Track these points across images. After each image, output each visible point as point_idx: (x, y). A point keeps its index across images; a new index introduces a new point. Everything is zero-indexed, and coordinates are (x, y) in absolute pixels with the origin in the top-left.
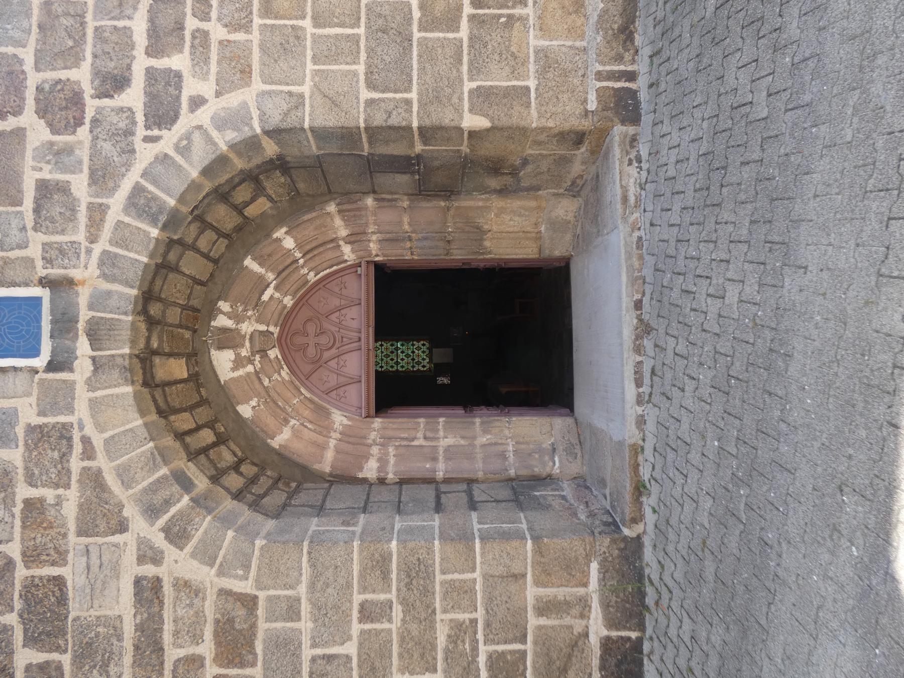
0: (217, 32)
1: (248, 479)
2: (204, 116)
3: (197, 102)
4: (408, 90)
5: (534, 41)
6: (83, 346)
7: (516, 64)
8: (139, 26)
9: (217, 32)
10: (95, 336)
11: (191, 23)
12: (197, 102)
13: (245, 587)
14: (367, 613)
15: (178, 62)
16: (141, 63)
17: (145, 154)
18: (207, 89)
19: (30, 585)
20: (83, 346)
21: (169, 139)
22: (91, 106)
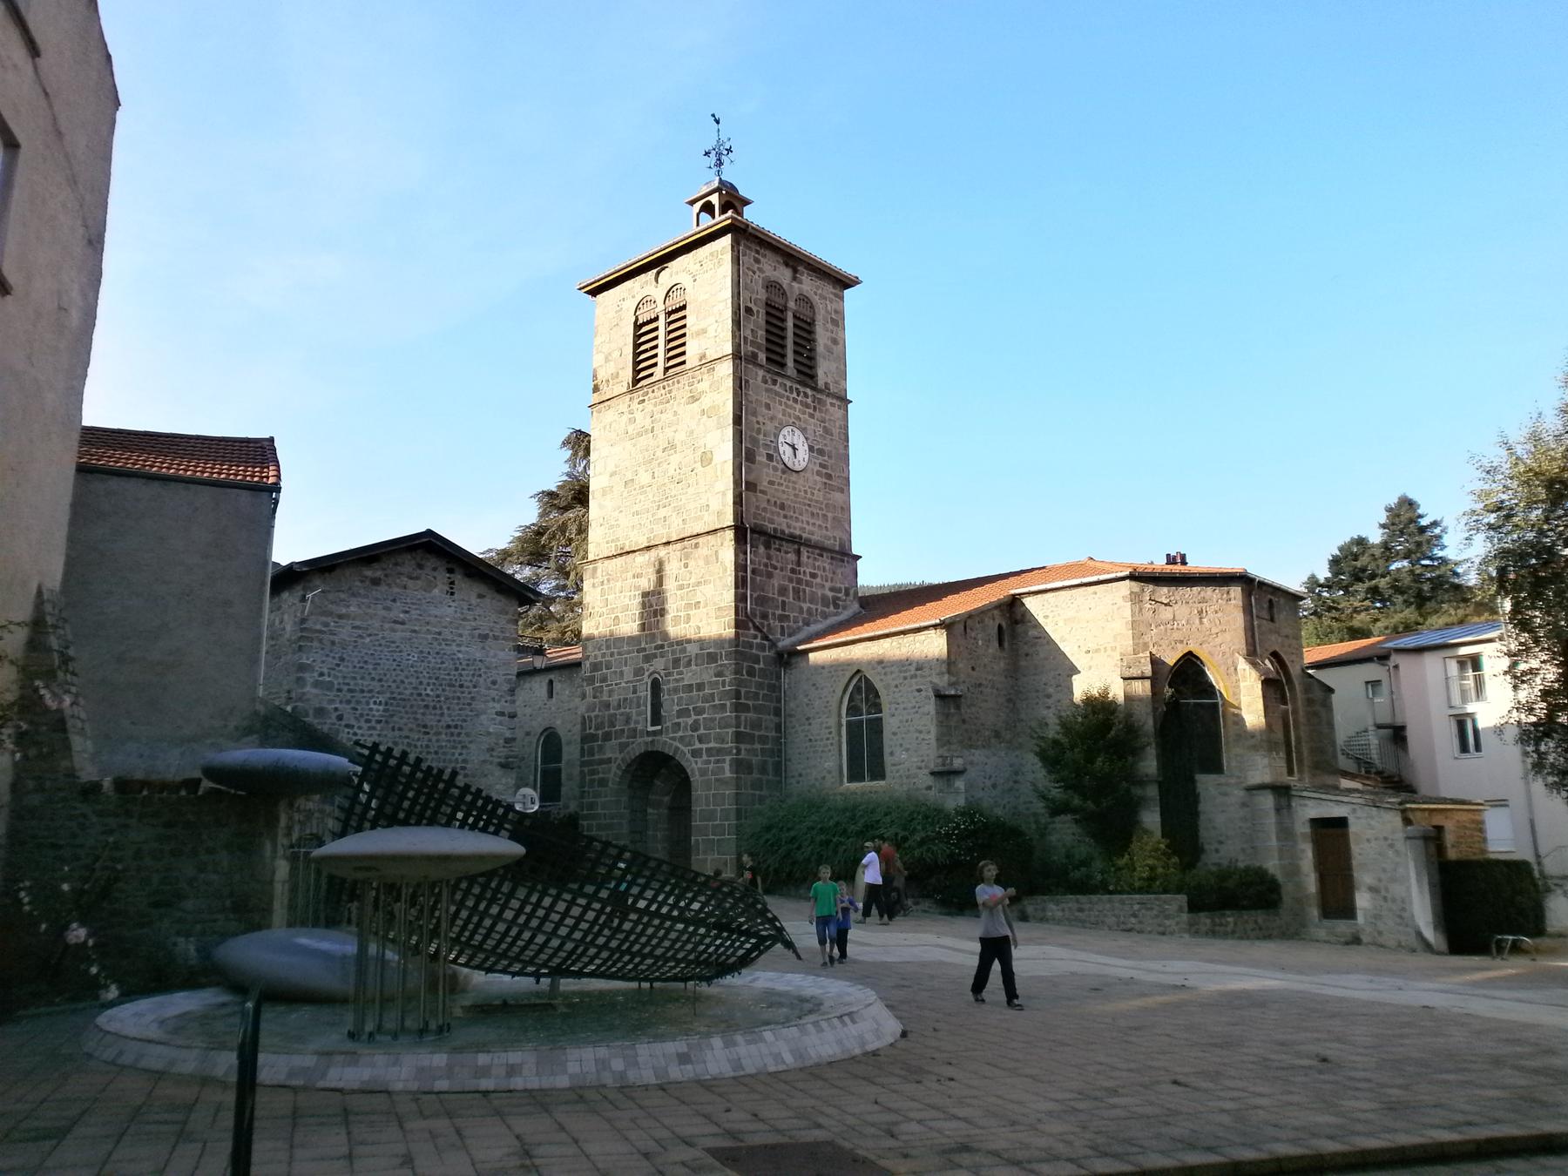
0: (711, 766)
1: (507, 908)
2: (694, 765)
3: (696, 763)
4: (705, 729)
5: (709, 858)
6: (650, 739)
7: (705, 852)
8: (712, 745)
9: (711, 766)
10: (652, 742)
11: (712, 759)
12: (696, 763)
13: (610, 784)
14: (724, 682)
15: (705, 757)
16: (704, 746)
17: (686, 750)
18: (700, 765)
19: (756, 688)
20: (650, 739)
21: (689, 756)
22: (695, 734)
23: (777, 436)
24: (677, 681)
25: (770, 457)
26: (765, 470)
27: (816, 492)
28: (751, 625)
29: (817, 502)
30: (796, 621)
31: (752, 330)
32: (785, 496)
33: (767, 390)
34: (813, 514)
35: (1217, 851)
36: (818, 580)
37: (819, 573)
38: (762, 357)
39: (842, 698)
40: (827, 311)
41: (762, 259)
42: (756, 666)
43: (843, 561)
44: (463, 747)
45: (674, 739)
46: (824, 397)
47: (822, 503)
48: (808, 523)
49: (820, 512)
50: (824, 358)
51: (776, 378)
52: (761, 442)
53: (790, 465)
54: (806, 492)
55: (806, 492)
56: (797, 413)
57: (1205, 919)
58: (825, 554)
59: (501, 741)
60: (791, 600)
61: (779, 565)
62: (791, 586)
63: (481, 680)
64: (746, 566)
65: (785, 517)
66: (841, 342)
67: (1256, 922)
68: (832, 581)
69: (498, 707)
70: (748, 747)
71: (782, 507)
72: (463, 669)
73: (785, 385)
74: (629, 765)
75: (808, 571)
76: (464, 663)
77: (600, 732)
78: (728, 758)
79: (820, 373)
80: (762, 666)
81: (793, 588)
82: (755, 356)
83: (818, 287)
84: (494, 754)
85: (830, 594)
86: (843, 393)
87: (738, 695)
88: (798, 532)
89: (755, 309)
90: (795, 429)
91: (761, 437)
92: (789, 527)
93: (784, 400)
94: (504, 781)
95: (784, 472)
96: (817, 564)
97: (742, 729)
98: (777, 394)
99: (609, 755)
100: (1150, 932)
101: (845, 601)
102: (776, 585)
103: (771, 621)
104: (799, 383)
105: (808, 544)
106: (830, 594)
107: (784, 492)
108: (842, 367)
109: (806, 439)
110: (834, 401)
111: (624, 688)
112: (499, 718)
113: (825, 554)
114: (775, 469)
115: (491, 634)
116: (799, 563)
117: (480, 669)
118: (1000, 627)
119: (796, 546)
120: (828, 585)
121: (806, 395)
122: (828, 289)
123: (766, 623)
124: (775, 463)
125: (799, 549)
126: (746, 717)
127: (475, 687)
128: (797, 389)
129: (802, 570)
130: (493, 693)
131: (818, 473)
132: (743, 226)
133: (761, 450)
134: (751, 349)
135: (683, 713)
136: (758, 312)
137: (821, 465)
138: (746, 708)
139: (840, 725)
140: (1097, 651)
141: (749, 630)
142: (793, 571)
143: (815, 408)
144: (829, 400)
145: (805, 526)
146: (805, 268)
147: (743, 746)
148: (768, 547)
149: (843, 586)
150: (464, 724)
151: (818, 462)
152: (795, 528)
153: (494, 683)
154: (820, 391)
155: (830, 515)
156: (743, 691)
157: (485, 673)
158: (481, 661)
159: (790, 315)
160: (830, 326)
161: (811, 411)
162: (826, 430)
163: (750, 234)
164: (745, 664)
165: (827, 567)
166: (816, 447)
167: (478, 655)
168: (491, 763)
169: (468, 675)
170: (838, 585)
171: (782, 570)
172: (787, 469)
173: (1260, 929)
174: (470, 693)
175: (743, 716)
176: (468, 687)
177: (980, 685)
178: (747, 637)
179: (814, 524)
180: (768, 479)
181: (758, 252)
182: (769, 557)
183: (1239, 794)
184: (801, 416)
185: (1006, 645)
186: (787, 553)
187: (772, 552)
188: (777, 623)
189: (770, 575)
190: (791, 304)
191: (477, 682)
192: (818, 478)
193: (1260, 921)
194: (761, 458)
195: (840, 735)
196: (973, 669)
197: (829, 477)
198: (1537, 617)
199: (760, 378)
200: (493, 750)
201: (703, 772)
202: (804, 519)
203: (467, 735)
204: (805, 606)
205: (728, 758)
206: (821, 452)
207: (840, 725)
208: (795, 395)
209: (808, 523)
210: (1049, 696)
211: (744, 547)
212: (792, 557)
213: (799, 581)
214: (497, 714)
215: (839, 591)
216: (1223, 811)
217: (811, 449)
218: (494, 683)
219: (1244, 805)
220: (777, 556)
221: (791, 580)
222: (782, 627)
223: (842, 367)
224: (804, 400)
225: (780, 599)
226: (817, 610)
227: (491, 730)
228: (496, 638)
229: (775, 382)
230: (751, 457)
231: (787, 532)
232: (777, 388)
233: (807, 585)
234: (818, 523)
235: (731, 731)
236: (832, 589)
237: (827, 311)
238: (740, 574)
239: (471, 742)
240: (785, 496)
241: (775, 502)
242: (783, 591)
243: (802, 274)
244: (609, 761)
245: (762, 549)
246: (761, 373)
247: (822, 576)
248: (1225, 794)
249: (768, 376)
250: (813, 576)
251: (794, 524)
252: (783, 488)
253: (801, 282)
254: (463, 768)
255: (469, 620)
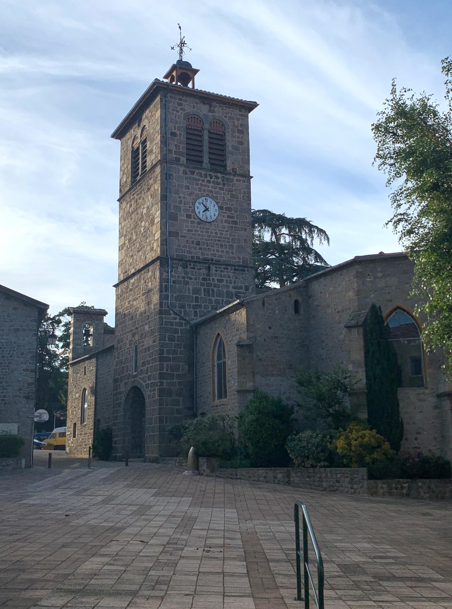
6: (133, 379)
23: (194, 204)
24: (142, 346)
25: (189, 216)
26: (185, 224)
27: (224, 233)
28: (171, 312)
29: (225, 238)
30: (206, 307)
31: (176, 145)
32: (200, 237)
33: (186, 178)
34: (221, 245)
35: (416, 439)
36: (224, 283)
37: (225, 279)
38: (183, 160)
39: (214, 350)
40: (234, 125)
41: (184, 103)
42: (176, 335)
43: (227, 269)
44: (3, 389)
45: (140, 379)
46: (232, 177)
47: (229, 239)
48: (218, 251)
49: (227, 244)
50: (232, 154)
51: (193, 170)
52: (182, 208)
53: (204, 219)
54: (216, 233)
55: (216, 233)
56: (210, 189)
57: (382, 485)
58: (229, 268)
59: (26, 385)
60: (203, 296)
61: (193, 277)
62: (202, 288)
63: (15, 353)
64: (168, 279)
65: (200, 249)
66: (246, 143)
67: (429, 487)
68: (235, 283)
69: (25, 366)
70: (169, 381)
71: (198, 243)
72: (4, 348)
73: (201, 174)
74: (128, 395)
75: (216, 278)
76: (5, 344)
77: (119, 377)
78: (157, 388)
79: (229, 163)
80: (180, 335)
81: (204, 289)
82: (177, 160)
83: (227, 113)
84: (22, 391)
85: (233, 291)
86: (247, 173)
87: (161, 352)
88: (210, 257)
89: (178, 133)
90: (208, 198)
91: (182, 205)
92: (202, 254)
93: (201, 182)
94: (27, 406)
95: (199, 223)
96: (223, 274)
97: (165, 371)
98: (194, 179)
99: (122, 390)
100: (347, 492)
101: (245, 293)
102: (191, 288)
103: (187, 309)
104: (211, 171)
105: (218, 263)
106: (233, 291)
107: (199, 235)
108: (247, 158)
109: (217, 203)
110: (240, 178)
111: (127, 352)
112: (24, 372)
113: (229, 268)
114: (192, 222)
115: (21, 328)
116: (209, 275)
117: (14, 347)
118: (296, 302)
119: (207, 265)
120: (231, 285)
121: (217, 178)
122: (236, 112)
123: (183, 310)
124: (192, 219)
125: (209, 267)
126: (167, 365)
127: (11, 357)
128: (209, 175)
129: (211, 278)
130: (22, 360)
131: (226, 221)
132: (165, 86)
133: (182, 212)
134: (175, 156)
135: (144, 364)
136: (180, 134)
137: (228, 217)
138: (168, 359)
139: (213, 366)
140: (343, 311)
141: (170, 314)
142: (204, 279)
143: (224, 184)
144: (235, 178)
145: (215, 252)
146: (217, 103)
147: (165, 381)
148: (185, 267)
149: (243, 285)
150: (4, 377)
151: (226, 215)
152: (208, 255)
153: (22, 354)
154: (229, 174)
155: (235, 245)
156: (165, 349)
157: (17, 349)
158: (15, 343)
159: (206, 133)
160: (237, 134)
161: (221, 186)
162: (233, 196)
163: (171, 89)
164: (167, 334)
165: (231, 275)
166: (225, 207)
167: (13, 340)
168: (20, 397)
169: (7, 351)
170: (240, 285)
171: (196, 279)
172: (201, 222)
173: (433, 492)
174: (8, 360)
175: (165, 364)
176: (7, 357)
177: (276, 337)
178: (168, 318)
179: (222, 251)
180: (187, 229)
181: (180, 99)
182: (186, 273)
183: (433, 400)
184: (213, 190)
185: (302, 312)
186: (200, 269)
187: (188, 270)
188: (191, 309)
189: (186, 283)
190: (207, 126)
191: (13, 354)
192: (226, 224)
193: (433, 486)
194: (182, 217)
195: (213, 373)
196: (270, 328)
197: (235, 223)
198: (409, 250)
199: (181, 172)
200: (21, 390)
201: (149, 396)
202: (215, 249)
203: (6, 382)
204: (213, 299)
205: (157, 388)
206: (229, 209)
207: (213, 366)
208: (209, 178)
209: (218, 251)
210: (323, 342)
211: (166, 269)
212: (204, 271)
213: (209, 285)
214: (24, 370)
215: (241, 288)
216: (421, 412)
217: (221, 208)
218: (22, 354)
219: (436, 407)
220: (192, 272)
221: (202, 285)
222: (196, 312)
223: (247, 158)
224: (216, 180)
225: (194, 296)
226: (223, 300)
227: (20, 379)
228: (24, 330)
229: (193, 173)
230: (173, 217)
231: (201, 257)
232: (194, 176)
233: (215, 286)
234: (225, 250)
235: (158, 372)
236: (234, 288)
237: (234, 125)
238: (164, 284)
239: (8, 386)
240: (200, 237)
241: (193, 242)
242: (196, 291)
243: (215, 107)
244: (121, 393)
245: (180, 269)
246: (182, 169)
247: (227, 281)
248: (423, 400)
249: (187, 170)
250: (220, 281)
251: (207, 252)
252: (199, 233)
253: (214, 112)
254: (280, 394)
255: (8, 322)
